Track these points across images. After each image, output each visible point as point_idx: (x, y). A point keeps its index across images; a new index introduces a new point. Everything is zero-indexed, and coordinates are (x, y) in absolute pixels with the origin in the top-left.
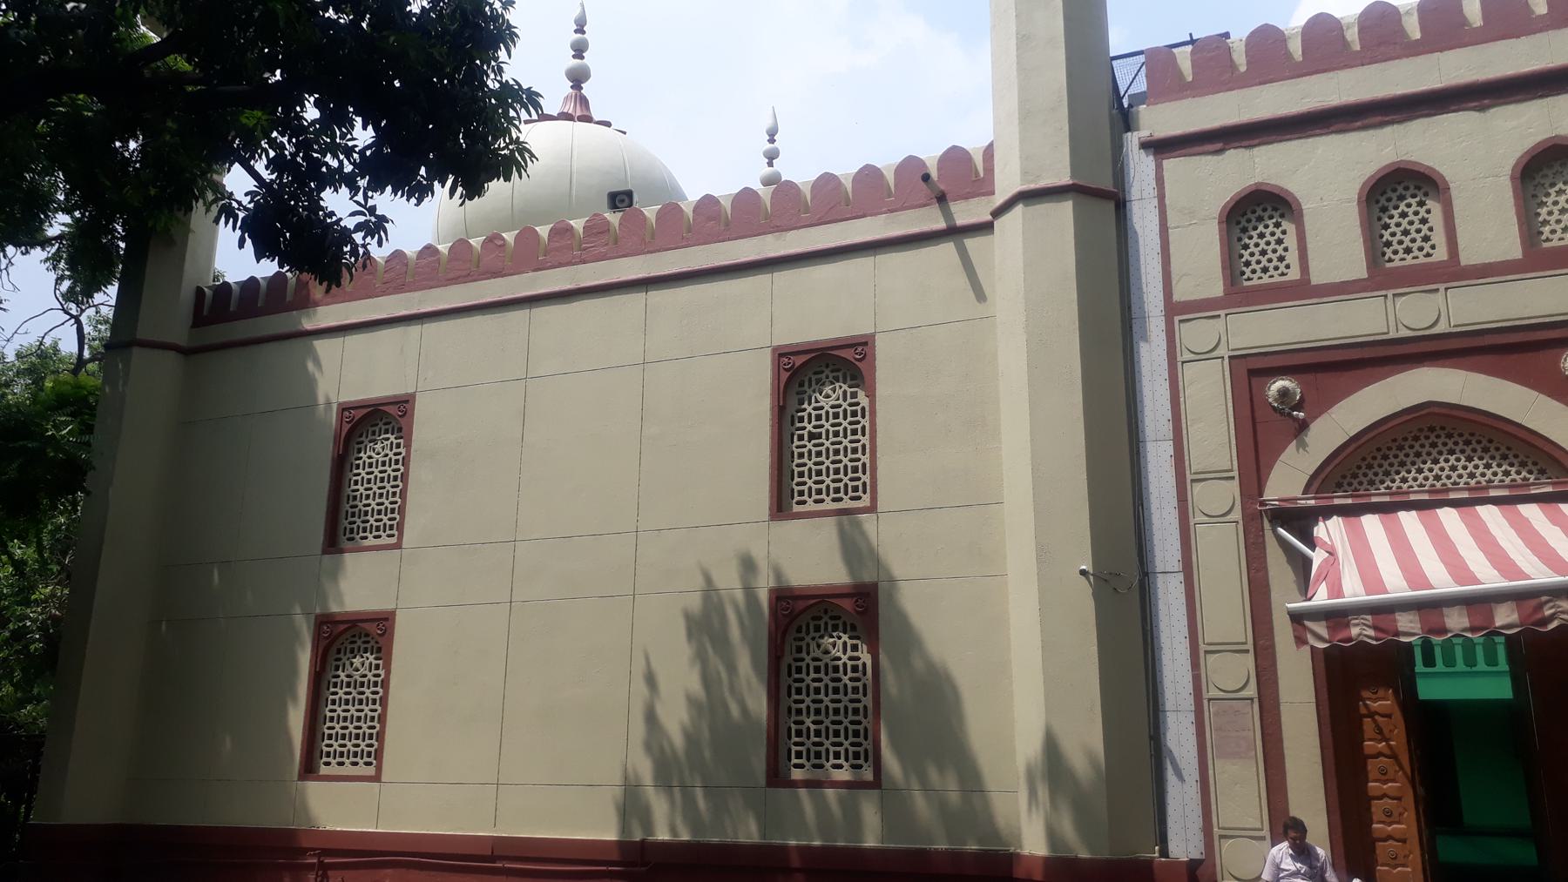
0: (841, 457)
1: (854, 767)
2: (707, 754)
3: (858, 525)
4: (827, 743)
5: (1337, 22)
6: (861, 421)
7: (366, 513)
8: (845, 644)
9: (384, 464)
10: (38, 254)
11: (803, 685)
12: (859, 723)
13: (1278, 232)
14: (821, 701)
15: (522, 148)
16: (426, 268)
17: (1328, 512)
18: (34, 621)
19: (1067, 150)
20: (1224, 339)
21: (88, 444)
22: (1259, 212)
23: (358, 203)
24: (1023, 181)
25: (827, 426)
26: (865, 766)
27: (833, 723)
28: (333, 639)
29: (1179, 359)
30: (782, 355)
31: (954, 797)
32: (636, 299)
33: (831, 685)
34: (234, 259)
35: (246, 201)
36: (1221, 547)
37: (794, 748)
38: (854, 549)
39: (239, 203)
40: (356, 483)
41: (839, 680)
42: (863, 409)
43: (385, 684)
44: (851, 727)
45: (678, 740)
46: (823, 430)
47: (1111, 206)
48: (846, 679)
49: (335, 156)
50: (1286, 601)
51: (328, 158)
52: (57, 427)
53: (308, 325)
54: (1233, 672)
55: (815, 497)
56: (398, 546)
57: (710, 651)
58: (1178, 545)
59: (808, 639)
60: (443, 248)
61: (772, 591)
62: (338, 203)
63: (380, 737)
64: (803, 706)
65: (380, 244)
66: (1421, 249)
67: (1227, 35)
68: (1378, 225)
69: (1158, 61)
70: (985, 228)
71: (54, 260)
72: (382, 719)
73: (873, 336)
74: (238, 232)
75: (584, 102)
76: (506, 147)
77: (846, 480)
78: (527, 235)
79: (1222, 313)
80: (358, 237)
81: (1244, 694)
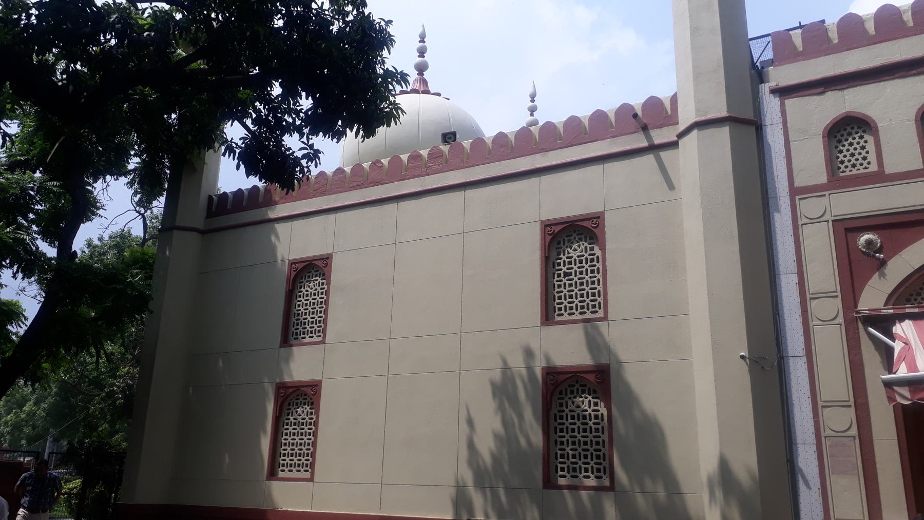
0: (585, 287)
1: (596, 477)
2: (506, 468)
3: (597, 328)
4: (580, 463)
5: (897, 9)
6: (597, 266)
7: (305, 323)
8: (590, 401)
9: (315, 295)
10: (123, 180)
11: (564, 427)
12: (600, 450)
13: (862, 142)
14: (576, 437)
15: (397, 107)
16: (340, 181)
17: (902, 318)
18: (118, 387)
19: (724, 95)
20: (828, 210)
21: (150, 285)
22: (849, 129)
23: (303, 142)
24: (697, 116)
25: (575, 268)
26: (604, 477)
27: (584, 450)
28: (286, 397)
29: (800, 222)
30: (547, 226)
31: (662, 496)
32: (458, 196)
33: (582, 427)
34: (230, 177)
35: (240, 143)
36: (831, 341)
37: (560, 466)
38: (594, 343)
39: (237, 144)
40: (299, 306)
41: (587, 424)
42: (598, 257)
43: (316, 424)
44: (595, 453)
45: (488, 460)
46: (573, 271)
47: (753, 129)
48: (591, 423)
49: (290, 115)
50: (875, 375)
51: (286, 117)
52: (133, 276)
53: (272, 215)
54: (841, 420)
55: (568, 311)
56: (323, 342)
57: (507, 405)
58: (802, 339)
59: (566, 399)
60: (348, 169)
61: (543, 369)
62: (292, 142)
63: (313, 455)
64: (564, 440)
65: (316, 166)
66: (861, 164)
67: (823, 21)
68: (836, 151)
69: (781, 40)
70: (673, 145)
71: (131, 184)
72: (314, 444)
73: (603, 213)
74: (236, 161)
75: (425, 82)
76: (388, 107)
77: (588, 301)
78: (395, 160)
79: (827, 193)
80: (304, 162)
81: (849, 433)
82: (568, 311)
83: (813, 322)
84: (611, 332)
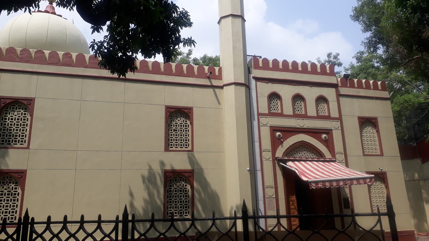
54: (271, 192)
57: (151, 186)
73: (34, 99)
81: (273, 197)
82: (175, 146)
83: (264, 159)
84: (197, 156)
